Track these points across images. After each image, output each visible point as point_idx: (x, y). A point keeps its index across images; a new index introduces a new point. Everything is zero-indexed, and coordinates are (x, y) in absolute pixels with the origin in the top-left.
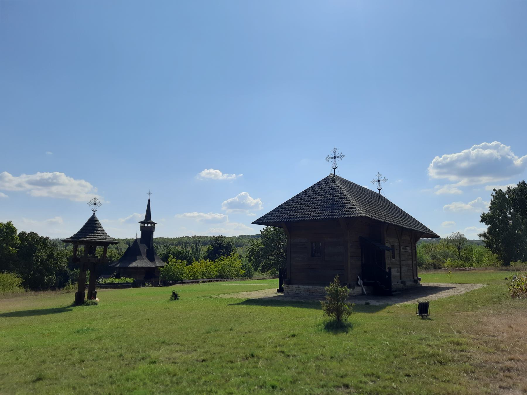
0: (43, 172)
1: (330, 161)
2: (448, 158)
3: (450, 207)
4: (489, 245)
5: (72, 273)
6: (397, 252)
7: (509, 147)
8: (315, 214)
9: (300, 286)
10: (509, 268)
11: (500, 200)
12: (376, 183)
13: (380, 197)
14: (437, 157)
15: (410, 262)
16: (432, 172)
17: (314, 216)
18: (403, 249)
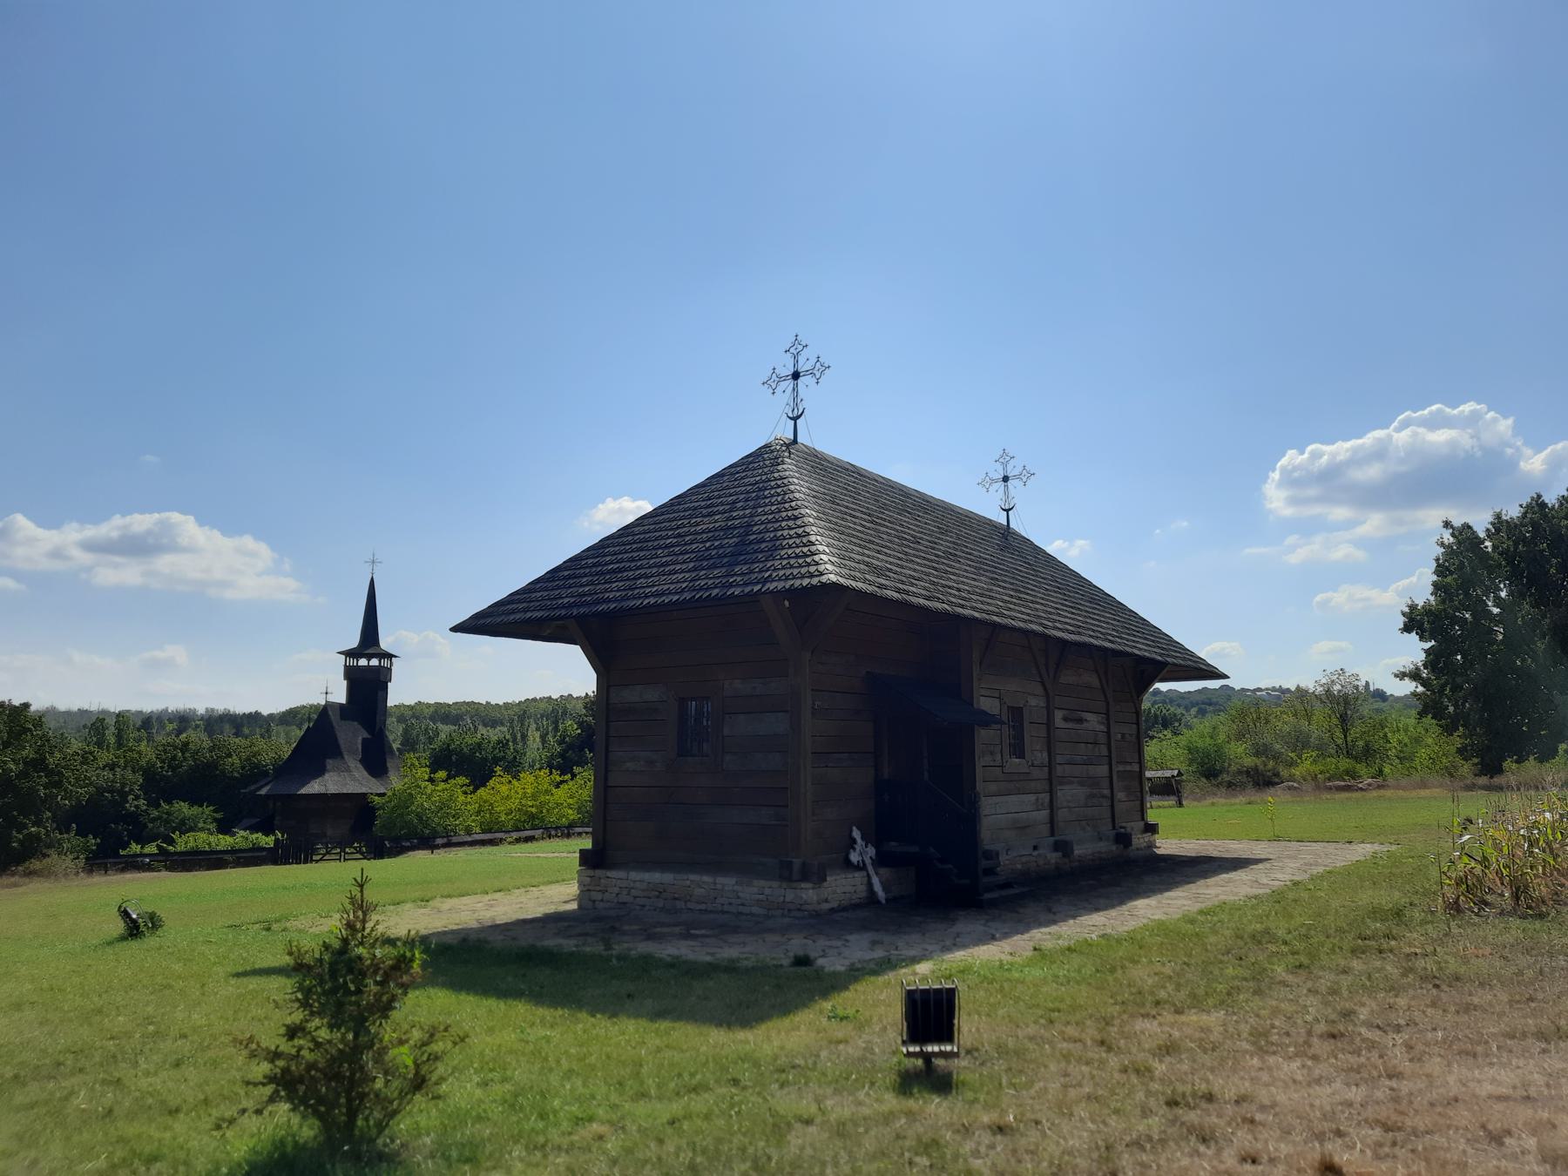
0: (130, 513)
1: (779, 390)
2: (1321, 455)
3: (1287, 583)
4: (1429, 706)
5: (155, 813)
6: (1033, 737)
7: (1510, 421)
8: (668, 584)
9: (634, 875)
10: (1497, 780)
11: (1463, 562)
12: (996, 486)
13: (1006, 537)
14: (1291, 453)
15: (1103, 770)
16: (1275, 497)
17: (663, 594)
18: (1065, 719)
